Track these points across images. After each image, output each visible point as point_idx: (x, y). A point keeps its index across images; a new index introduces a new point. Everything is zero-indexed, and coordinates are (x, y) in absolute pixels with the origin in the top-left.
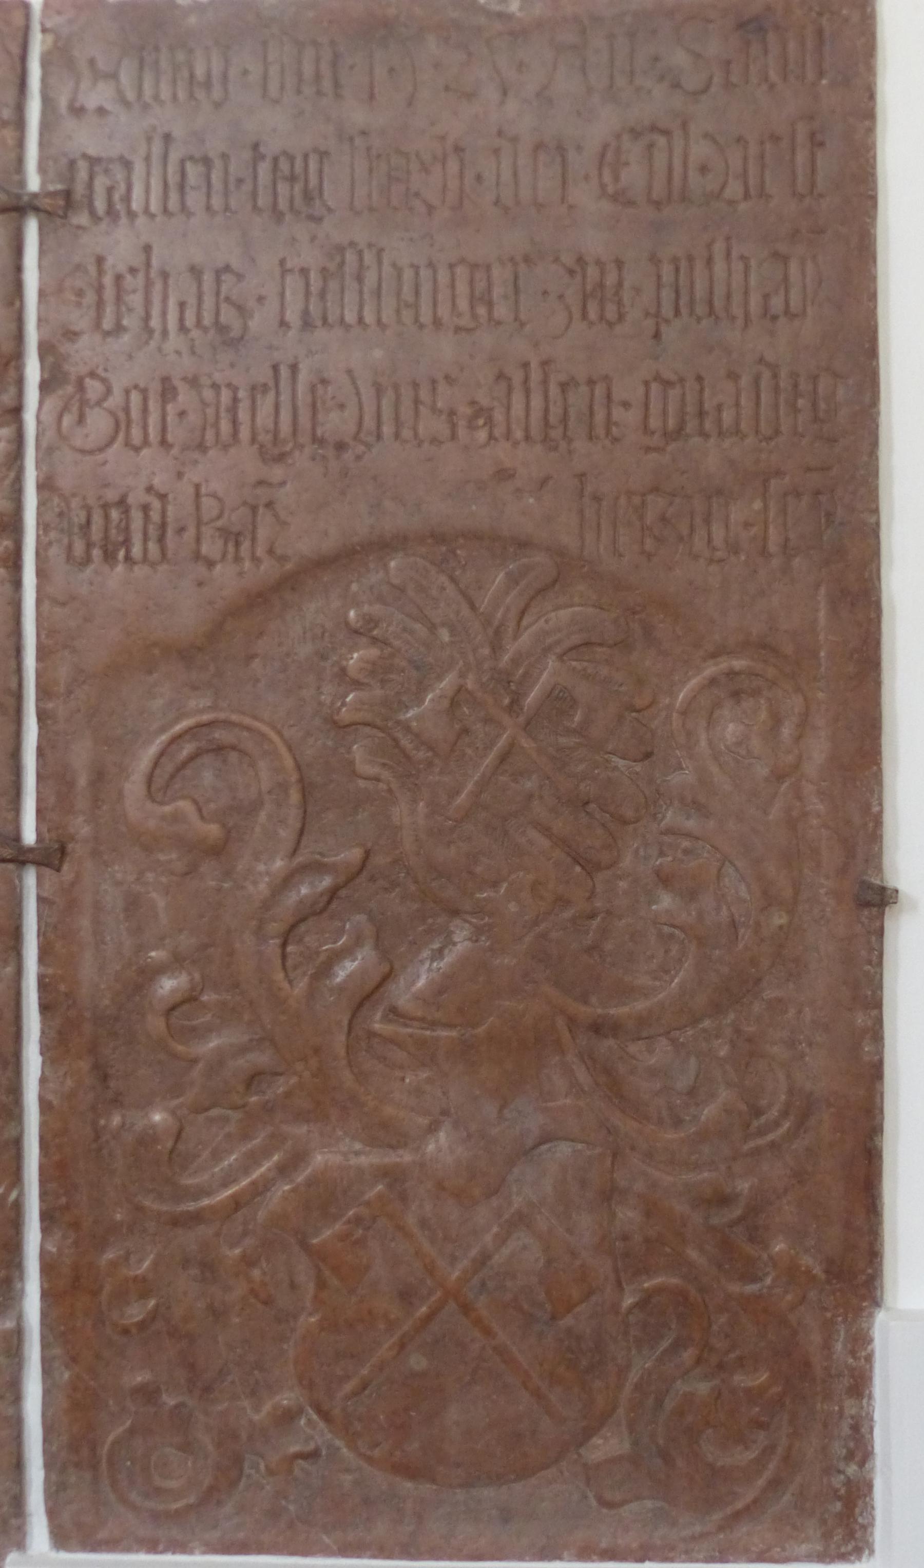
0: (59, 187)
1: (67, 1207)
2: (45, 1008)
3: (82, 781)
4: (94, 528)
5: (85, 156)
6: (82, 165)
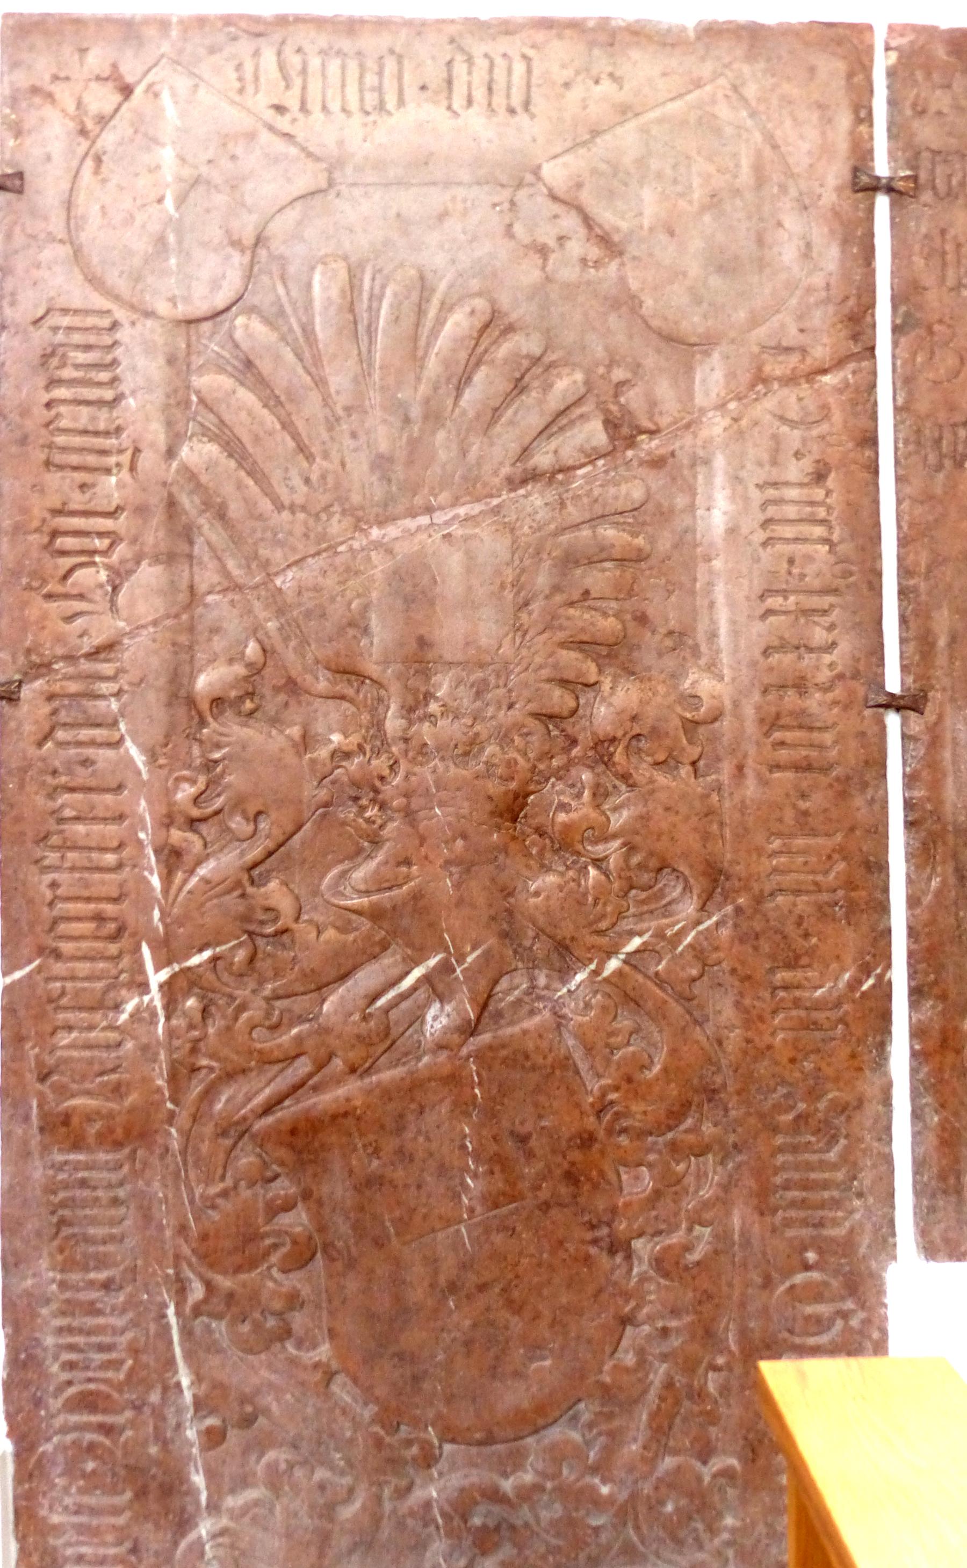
0: (908, 173)
1: (936, 982)
2: (910, 825)
3: (942, 642)
4: (944, 442)
5: (928, 149)
6: (926, 155)
